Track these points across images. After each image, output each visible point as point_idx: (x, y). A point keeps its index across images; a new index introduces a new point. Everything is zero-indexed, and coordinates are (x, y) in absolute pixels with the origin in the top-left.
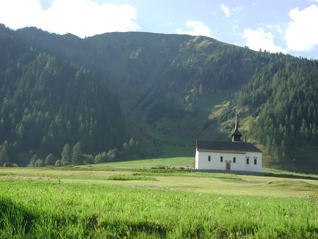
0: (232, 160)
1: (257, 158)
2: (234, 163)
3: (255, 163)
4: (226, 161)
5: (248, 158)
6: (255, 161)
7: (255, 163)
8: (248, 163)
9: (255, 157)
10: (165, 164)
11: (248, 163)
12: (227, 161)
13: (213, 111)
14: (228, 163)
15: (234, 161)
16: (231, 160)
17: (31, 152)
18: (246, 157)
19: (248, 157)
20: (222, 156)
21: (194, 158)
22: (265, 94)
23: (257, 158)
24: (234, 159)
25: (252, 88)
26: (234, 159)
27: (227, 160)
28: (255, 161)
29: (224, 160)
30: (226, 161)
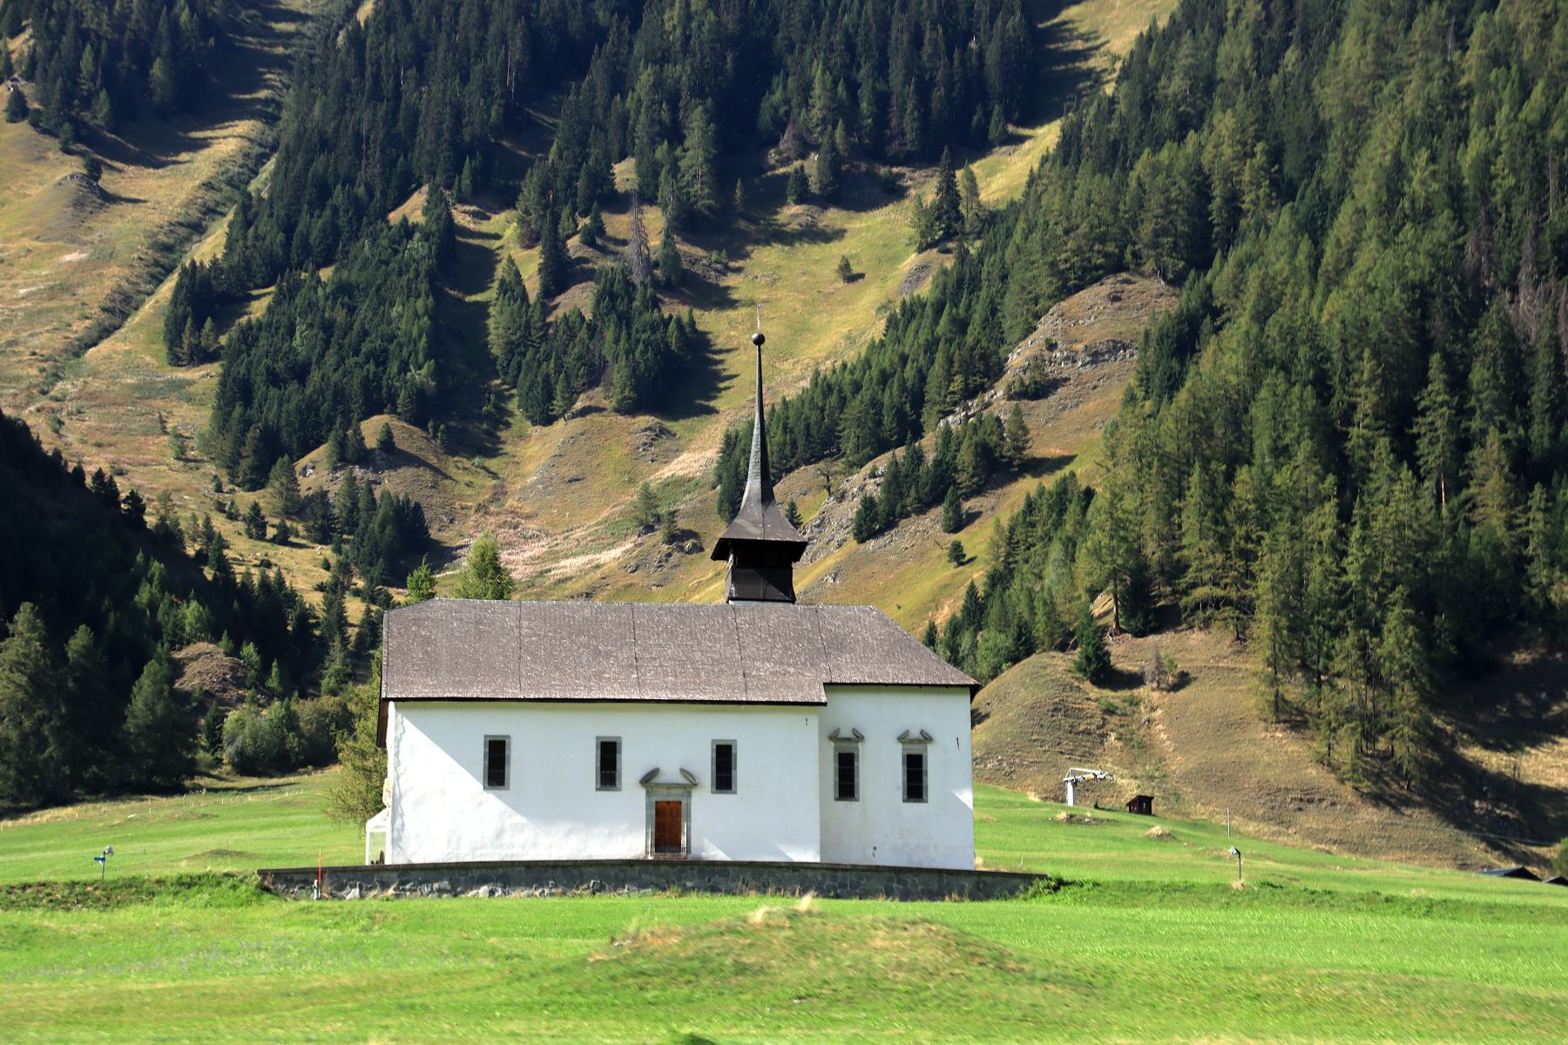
0: (705, 769)
1: (926, 738)
2: (724, 798)
3: (915, 788)
4: (648, 780)
5: (915, 749)
6: (915, 770)
7: (915, 788)
8: (846, 786)
9: (915, 734)
10: (1328, 852)
11: (846, 786)
12: (660, 779)
13: (217, 138)
14: (663, 795)
15: (724, 777)
16: (693, 769)
17: (689, 884)
18: (834, 737)
19: (846, 732)
20: (725, 736)
21: (842, 751)
22: (467, 138)
23: (926, 738)
24: (724, 757)
25: (176, 10)
26: (724, 757)
27: (654, 773)
28: (915, 770)
29: (631, 767)
30: (648, 780)
